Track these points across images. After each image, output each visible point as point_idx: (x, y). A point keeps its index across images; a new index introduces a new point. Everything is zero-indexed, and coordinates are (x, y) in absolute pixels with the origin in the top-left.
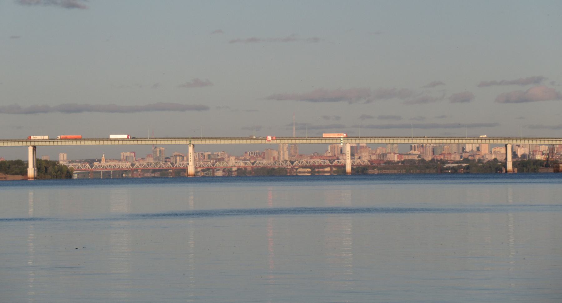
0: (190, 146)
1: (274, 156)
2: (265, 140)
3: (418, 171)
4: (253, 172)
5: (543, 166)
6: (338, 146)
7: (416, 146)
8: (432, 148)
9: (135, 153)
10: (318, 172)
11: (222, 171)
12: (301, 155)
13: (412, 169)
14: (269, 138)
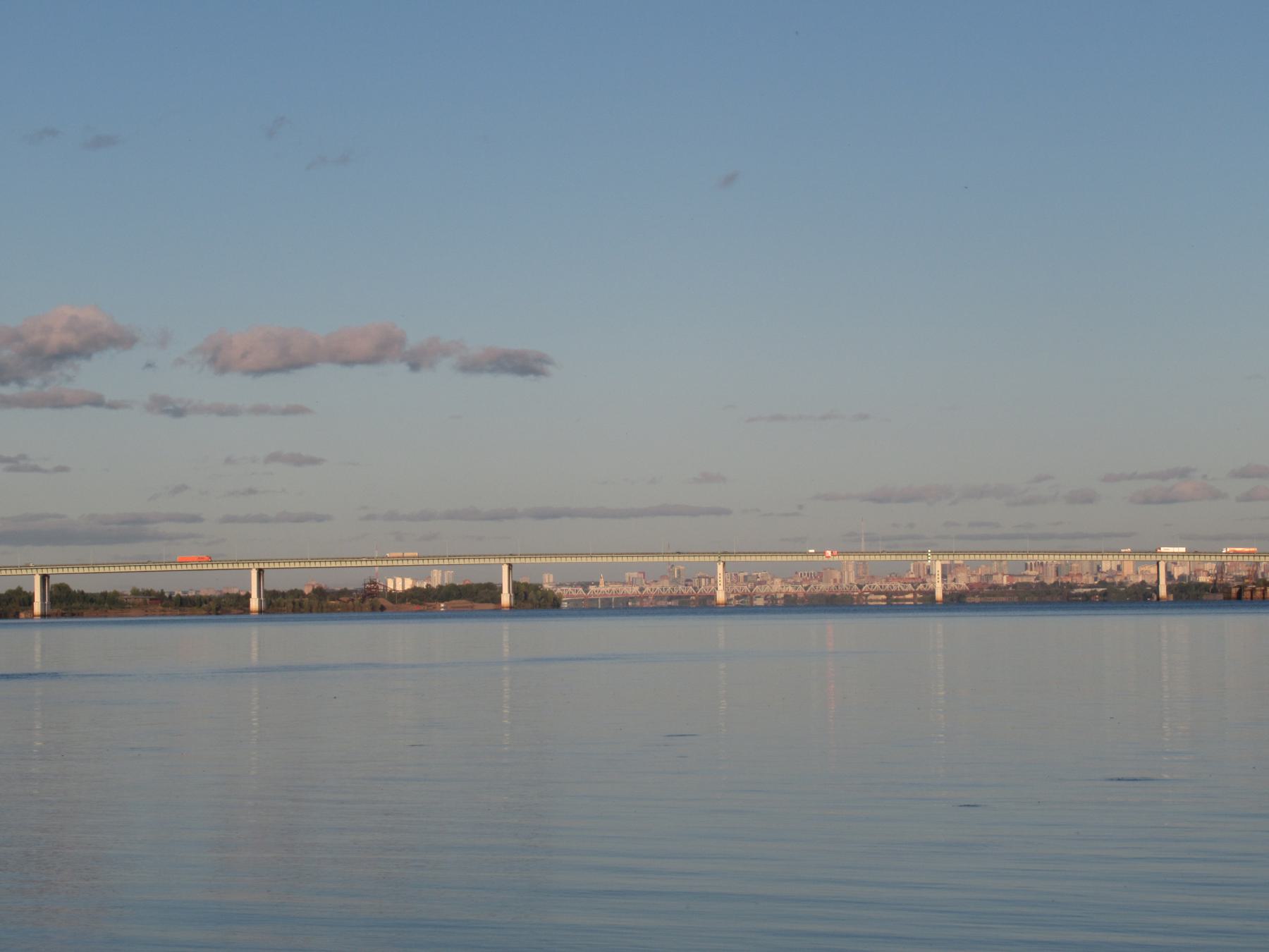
14: (829, 553)
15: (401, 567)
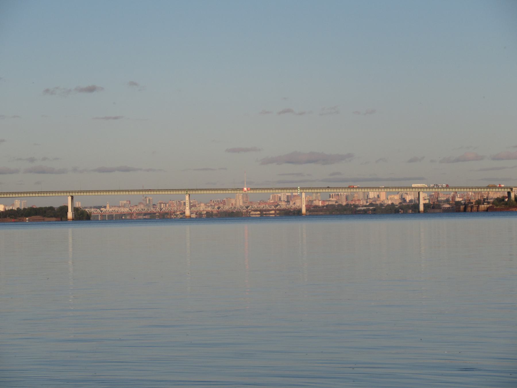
0: (187, 195)
1: (232, 203)
2: (242, 190)
3: (338, 213)
4: (219, 215)
5: (430, 208)
6: (278, 195)
7: (334, 195)
8: (346, 196)
9: (130, 201)
10: (265, 214)
11: (195, 214)
12: (251, 202)
13: (334, 211)
14: (245, 189)
15: (26, 197)
